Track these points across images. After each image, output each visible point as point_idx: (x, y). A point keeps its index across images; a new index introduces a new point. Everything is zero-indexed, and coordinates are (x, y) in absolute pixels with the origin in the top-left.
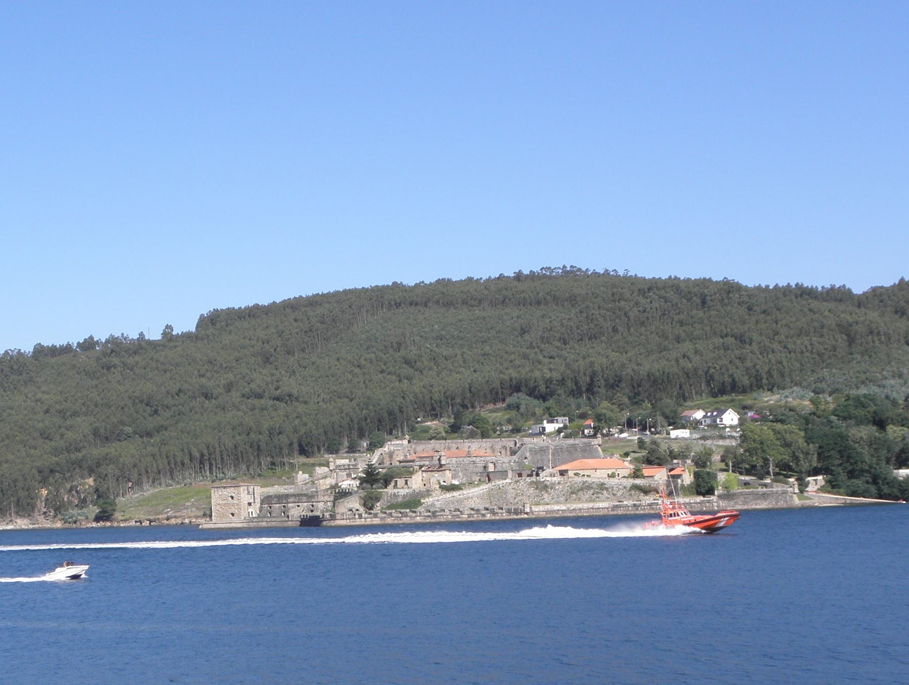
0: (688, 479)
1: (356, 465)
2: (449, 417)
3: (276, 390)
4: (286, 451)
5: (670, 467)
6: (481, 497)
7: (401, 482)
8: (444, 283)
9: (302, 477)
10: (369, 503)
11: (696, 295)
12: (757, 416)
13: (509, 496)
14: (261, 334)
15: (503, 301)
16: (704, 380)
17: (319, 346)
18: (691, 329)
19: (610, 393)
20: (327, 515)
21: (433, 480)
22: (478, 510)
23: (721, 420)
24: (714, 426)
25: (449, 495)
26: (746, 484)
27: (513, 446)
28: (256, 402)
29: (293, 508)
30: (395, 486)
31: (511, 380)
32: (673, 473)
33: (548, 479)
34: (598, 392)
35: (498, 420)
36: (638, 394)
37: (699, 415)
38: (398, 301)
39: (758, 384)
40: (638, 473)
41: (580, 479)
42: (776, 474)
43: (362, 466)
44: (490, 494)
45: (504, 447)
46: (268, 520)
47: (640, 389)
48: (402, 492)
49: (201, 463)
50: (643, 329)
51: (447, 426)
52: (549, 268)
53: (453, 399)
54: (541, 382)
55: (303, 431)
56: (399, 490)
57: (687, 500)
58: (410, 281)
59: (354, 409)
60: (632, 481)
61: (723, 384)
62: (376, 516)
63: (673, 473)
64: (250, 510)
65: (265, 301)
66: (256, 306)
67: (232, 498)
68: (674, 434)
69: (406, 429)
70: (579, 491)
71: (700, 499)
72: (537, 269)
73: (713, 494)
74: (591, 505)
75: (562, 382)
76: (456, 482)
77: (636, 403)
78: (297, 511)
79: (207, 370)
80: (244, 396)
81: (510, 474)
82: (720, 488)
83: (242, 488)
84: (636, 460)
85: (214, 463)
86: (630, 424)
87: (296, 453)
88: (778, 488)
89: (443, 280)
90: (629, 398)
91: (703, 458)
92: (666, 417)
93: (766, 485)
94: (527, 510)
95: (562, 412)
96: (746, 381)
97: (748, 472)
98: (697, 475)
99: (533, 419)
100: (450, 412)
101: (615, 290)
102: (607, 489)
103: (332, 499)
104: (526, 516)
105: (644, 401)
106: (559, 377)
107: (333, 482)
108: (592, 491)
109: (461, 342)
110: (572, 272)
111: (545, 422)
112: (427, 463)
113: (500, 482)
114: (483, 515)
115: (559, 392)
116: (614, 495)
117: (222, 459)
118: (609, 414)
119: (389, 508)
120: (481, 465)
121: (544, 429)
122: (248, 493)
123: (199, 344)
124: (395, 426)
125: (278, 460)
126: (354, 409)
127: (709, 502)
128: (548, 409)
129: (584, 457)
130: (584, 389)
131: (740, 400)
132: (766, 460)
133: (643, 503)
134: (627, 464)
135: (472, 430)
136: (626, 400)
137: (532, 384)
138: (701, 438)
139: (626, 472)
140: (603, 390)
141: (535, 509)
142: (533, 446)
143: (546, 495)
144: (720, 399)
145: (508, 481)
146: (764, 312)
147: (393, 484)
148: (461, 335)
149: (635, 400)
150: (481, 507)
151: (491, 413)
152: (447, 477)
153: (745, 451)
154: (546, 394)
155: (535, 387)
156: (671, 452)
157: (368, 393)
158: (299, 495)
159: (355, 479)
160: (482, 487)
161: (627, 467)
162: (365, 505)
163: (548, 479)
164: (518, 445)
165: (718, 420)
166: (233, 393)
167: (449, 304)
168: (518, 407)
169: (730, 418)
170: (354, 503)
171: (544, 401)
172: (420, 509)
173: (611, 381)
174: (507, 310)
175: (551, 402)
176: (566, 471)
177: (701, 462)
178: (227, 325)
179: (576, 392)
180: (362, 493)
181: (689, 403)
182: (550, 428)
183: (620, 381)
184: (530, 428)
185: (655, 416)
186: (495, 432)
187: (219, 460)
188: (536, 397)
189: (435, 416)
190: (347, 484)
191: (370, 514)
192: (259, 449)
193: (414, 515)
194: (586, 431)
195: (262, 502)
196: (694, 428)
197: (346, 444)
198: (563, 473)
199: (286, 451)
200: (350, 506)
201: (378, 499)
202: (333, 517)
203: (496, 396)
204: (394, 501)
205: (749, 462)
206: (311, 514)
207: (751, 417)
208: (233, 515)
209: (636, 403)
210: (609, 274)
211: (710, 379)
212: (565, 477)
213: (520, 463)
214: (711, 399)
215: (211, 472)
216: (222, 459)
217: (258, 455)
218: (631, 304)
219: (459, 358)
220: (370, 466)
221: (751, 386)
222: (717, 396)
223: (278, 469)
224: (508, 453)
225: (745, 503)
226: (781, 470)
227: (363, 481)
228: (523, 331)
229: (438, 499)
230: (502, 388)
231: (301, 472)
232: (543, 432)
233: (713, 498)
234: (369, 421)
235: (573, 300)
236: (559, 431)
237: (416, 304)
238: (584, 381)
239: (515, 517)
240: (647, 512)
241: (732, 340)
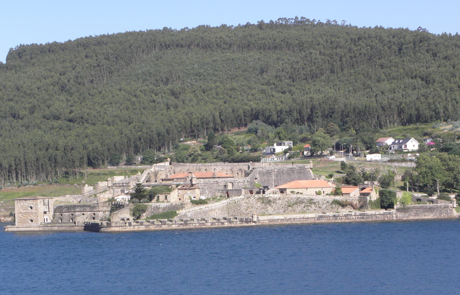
0: (374, 196)
1: (128, 183)
2: (205, 138)
3: (70, 113)
4: (77, 163)
5: (362, 187)
6: (221, 209)
7: (162, 197)
8: (203, 29)
9: (88, 189)
10: (137, 214)
11: (394, 44)
12: (432, 144)
13: (242, 208)
14: (59, 66)
15: (249, 45)
16: (396, 112)
17: (105, 79)
18: (390, 72)
19: (325, 122)
20: (105, 223)
21: (186, 197)
22: (219, 220)
23: (406, 146)
24: (400, 151)
25: (197, 208)
26: (419, 200)
27: (247, 169)
28: (56, 123)
29: (79, 216)
30: (158, 200)
31: (252, 110)
32: (364, 191)
33: (272, 195)
34: (316, 121)
35: (240, 141)
36: (346, 123)
37: (389, 141)
38: (168, 43)
39: (437, 117)
40: (338, 191)
41: (295, 196)
42: (442, 191)
43: (133, 184)
44: (228, 207)
45: (241, 170)
46: (59, 225)
47: (348, 119)
48: (163, 205)
49: (9, 172)
50: (352, 71)
51: (202, 145)
52: (285, 19)
53: (207, 124)
54: (274, 112)
55: (90, 147)
56: (160, 204)
57: (373, 212)
58: (177, 26)
59: (131, 131)
60: (333, 198)
61: (411, 115)
62: (142, 224)
63: (364, 191)
64: (46, 217)
65: (62, 40)
66: (55, 44)
67: (31, 208)
68: (369, 157)
69: (171, 147)
70: (294, 204)
71: (383, 211)
72: (275, 19)
73: (393, 208)
74: (302, 216)
75: (290, 113)
76: (203, 198)
77: (344, 129)
78: (82, 219)
79: (15, 96)
80: (44, 117)
81: (243, 191)
82: (398, 203)
83: (39, 201)
84: (338, 180)
85: (20, 172)
86: (338, 147)
87: (85, 165)
88: (442, 203)
89: (203, 26)
90: (339, 126)
91: (387, 180)
92: (365, 143)
93: (432, 201)
94: (255, 219)
95: (288, 137)
96: (428, 113)
97: (421, 189)
98: (381, 194)
99: (267, 141)
100: (205, 134)
101: (333, 39)
102: (314, 203)
103: (109, 209)
104: (254, 224)
105: (350, 128)
106: (288, 109)
107: (111, 196)
108: (303, 205)
109: (215, 78)
110: (301, 22)
111: (275, 144)
112: (182, 183)
113: (236, 198)
114: (223, 223)
115: (287, 120)
116: (320, 207)
117: (26, 169)
118: (321, 140)
119: (153, 217)
120: (223, 184)
121: (274, 150)
122: (44, 204)
123: (9, 73)
124: (163, 145)
125: (71, 170)
126: (131, 131)
127: (389, 214)
128: (279, 133)
129: (300, 179)
130: (306, 118)
131: (423, 128)
132: (435, 182)
133: (341, 214)
134: (330, 184)
135: (221, 150)
136: (337, 127)
137: (267, 114)
138: (389, 161)
139: (329, 191)
140: (320, 120)
141: (261, 218)
142: (261, 169)
143: (269, 208)
144: (408, 127)
145: (242, 197)
146: (446, 58)
147: (156, 198)
148: (216, 73)
149: (344, 127)
150: (221, 217)
151: (236, 136)
152: (197, 194)
153: (419, 174)
154: (278, 122)
155: (270, 116)
156: (364, 174)
157: (143, 118)
158: (84, 206)
159: (127, 194)
160: (222, 202)
161: (330, 186)
162: (134, 215)
163: (272, 195)
164: (251, 169)
165: (403, 146)
166: (35, 114)
167: (206, 47)
168: (256, 132)
169: (412, 145)
170: (126, 214)
171: (276, 127)
172: (176, 218)
173: (327, 112)
174: (251, 54)
175: (281, 129)
176: (285, 189)
177: (385, 183)
178: (31, 58)
179: (299, 121)
180: (132, 206)
181: (384, 130)
182: (279, 149)
183: (333, 113)
184: (264, 148)
185: (356, 142)
186: (238, 151)
187: (24, 170)
188: (270, 124)
189: (194, 137)
190: (122, 198)
191: (137, 222)
192: (56, 162)
193: (171, 223)
194: (305, 153)
195: (55, 211)
196: (385, 153)
197: (125, 157)
198: (282, 191)
199: (77, 163)
200: (122, 216)
201: (144, 211)
202: (109, 225)
203: (240, 123)
204: (156, 212)
205: (419, 183)
206: (92, 221)
207: (429, 144)
208: (32, 221)
209: (344, 129)
210: (330, 24)
211: (400, 112)
212: (284, 194)
213: (251, 183)
214: (401, 127)
215: (17, 179)
216: (26, 169)
217: (55, 167)
218: (346, 50)
219: (214, 91)
220: (138, 185)
221: (431, 117)
222: (406, 125)
223: (71, 178)
224: (244, 174)
225: (417, 214)
226: (446, 187)
227: (133, 196)
228: (262, 72)
229: (189, 211)
230: (245, 116)
231: (87, 185)
232: (273, 152)
233: (393, 211)
234: (142, 140)
235: (301, 46)
236: (285, 152)
237: (182, 46)
238: (306, 112)
239: (246, 224)
240: (343, 221)
241: (420, 82)
